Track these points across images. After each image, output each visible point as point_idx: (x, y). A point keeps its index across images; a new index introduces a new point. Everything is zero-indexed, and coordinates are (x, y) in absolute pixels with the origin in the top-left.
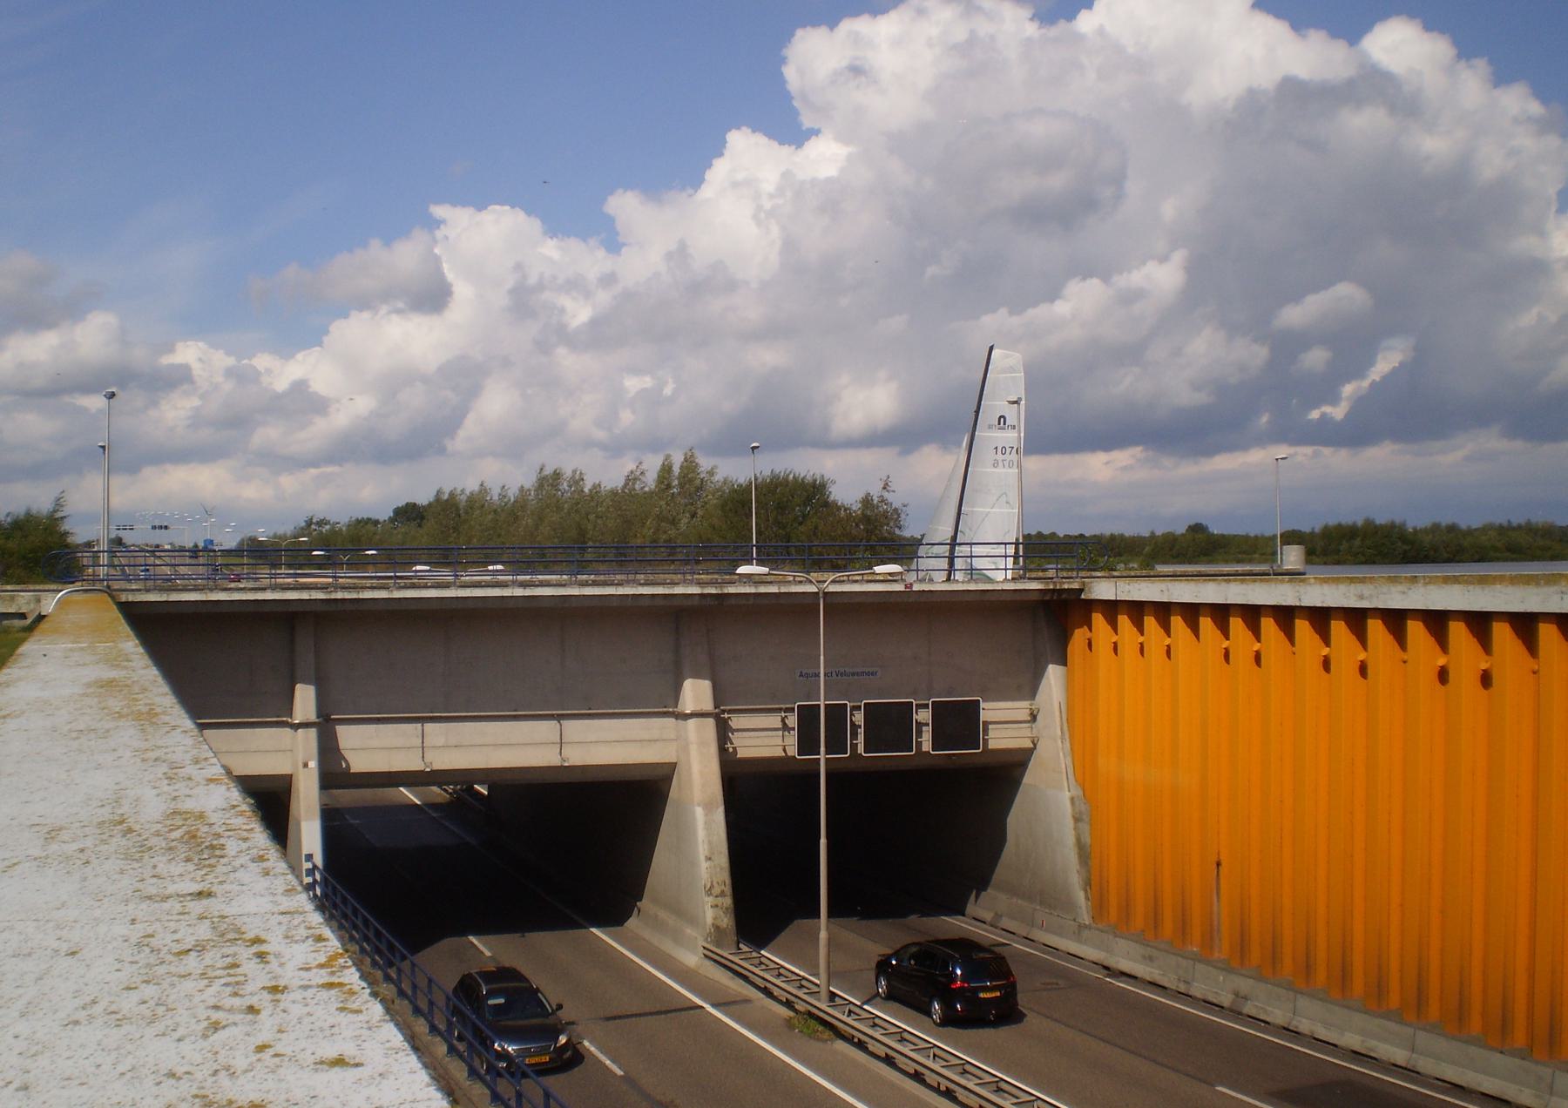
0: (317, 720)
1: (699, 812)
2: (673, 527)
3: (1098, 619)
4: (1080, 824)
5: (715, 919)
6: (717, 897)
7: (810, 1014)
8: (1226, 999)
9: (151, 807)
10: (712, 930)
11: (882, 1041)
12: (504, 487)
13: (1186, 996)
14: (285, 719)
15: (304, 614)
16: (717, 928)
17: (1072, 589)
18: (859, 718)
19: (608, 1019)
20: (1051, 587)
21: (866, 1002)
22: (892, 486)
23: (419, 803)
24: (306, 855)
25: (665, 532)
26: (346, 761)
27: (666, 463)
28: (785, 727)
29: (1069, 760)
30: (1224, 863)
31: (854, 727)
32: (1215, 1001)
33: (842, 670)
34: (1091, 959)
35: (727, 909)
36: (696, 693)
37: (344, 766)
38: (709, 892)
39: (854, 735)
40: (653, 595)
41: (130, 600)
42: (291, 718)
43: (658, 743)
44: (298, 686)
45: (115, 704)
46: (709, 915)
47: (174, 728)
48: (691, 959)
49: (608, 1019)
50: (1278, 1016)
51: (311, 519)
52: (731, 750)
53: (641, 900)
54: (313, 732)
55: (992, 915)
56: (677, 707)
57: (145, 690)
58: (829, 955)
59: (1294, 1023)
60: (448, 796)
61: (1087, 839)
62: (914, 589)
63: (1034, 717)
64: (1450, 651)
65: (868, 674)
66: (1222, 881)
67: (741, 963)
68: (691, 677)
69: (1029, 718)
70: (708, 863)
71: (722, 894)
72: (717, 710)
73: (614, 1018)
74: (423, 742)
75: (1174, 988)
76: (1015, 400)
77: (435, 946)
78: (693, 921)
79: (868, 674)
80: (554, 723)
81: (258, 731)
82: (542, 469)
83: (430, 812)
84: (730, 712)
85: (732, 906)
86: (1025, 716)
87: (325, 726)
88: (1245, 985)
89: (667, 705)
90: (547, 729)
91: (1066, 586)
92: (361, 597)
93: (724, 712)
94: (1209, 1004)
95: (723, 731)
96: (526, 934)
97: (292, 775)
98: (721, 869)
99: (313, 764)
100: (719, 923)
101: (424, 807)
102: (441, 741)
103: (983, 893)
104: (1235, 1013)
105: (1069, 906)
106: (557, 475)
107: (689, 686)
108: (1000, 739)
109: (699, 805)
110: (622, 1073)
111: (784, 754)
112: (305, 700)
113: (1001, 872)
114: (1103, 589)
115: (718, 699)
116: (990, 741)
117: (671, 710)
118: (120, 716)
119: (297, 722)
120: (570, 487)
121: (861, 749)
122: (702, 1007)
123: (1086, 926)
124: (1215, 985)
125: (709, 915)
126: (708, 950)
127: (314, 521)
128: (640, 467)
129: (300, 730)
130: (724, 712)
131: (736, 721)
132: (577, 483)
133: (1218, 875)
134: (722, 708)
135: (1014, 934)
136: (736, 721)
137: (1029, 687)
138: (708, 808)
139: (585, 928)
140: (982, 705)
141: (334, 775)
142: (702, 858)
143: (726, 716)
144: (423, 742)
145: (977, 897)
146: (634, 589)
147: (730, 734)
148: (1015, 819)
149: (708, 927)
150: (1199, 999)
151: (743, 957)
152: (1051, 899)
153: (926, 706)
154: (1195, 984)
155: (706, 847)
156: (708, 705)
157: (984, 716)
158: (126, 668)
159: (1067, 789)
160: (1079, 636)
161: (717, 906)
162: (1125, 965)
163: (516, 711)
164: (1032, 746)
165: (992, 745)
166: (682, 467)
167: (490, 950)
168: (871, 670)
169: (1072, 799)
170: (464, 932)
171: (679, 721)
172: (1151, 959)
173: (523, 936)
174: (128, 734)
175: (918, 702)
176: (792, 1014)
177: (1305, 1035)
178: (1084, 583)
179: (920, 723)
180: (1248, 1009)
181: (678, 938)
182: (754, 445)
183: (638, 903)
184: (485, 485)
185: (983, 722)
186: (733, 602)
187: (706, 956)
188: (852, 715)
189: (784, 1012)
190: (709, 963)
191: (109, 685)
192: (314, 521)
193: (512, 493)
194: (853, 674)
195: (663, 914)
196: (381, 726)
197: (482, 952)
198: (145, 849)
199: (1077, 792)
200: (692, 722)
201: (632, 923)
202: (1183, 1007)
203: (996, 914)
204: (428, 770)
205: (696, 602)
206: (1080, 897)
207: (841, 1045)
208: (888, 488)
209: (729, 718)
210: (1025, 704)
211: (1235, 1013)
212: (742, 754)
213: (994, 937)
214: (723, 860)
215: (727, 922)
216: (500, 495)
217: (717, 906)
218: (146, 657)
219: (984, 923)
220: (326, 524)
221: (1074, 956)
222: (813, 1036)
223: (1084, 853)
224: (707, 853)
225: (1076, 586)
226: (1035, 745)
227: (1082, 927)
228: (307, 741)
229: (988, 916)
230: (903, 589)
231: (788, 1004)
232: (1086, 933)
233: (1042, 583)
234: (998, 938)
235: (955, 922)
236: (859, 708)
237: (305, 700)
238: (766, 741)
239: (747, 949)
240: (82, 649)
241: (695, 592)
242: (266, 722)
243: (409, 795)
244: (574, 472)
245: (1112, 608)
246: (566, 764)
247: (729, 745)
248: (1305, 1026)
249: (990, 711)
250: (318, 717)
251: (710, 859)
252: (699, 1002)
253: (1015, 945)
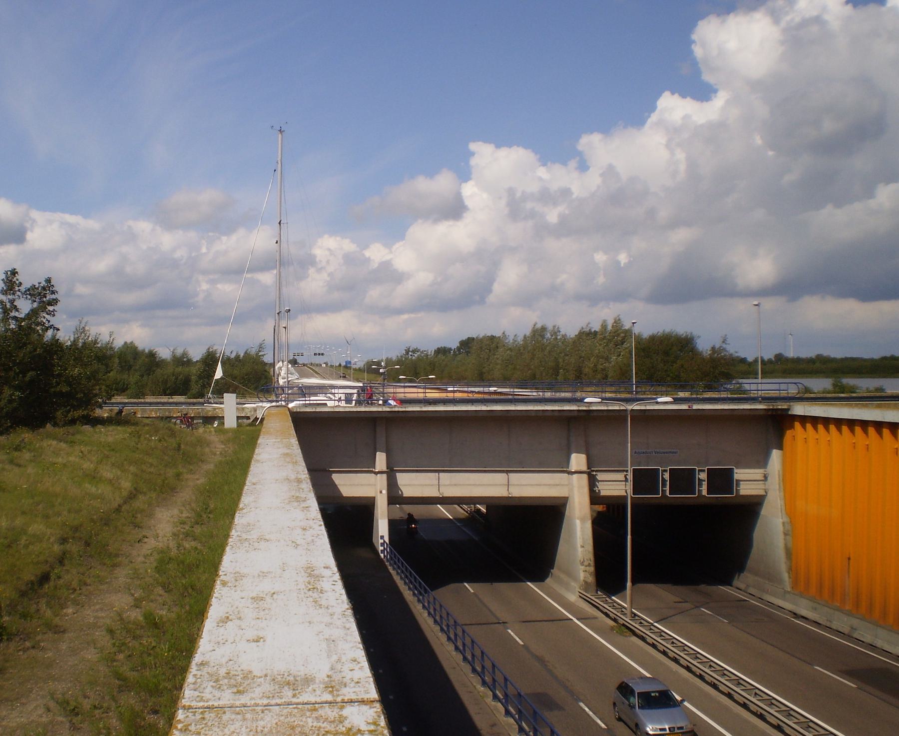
0: (387, 470)
1: (578, 522)
2: (606, 362)
3: (797, 425)
4: (788, 537)
5: (585, 577)
6: (586, 566)
7: (624, 625)
8: (846, 630)
9: (293, 477)
10: (583, 583)
11: (652, 637)
12: (516, 335)
13: (828, 629)
14: (371, 469)
15: (381, 418)
16: (586, 582)
17: (783, 409)
18: (667, 476)
19: (524, 622)
20: (771, 408)
21: (656, 622)
22: (728, 341)
23: (451, 518)
24: (381, 536)
25: (602, 364)
26: (401, 491)
27: (604, 324)
28: (626, 480)
29: (783, 503)
30: (852, 558)
31: (664, 480)
32: (842, 631)
33: (658, 450)
34: (789, 609)
35: (591, 573)
36: (578, 461)
37: (400, 493)
38: (582, 564)
39: (664, 485)
40: (553, 410)
41: (298, 411)
42: (375, 469)
43: (558, 486)
44: (378, 453)
45: (288, 460)
46: (582, 576)
47: (300, 465)
48: (573, 598)
49: (524, 622)
50: (868, 639)
51: (409, 349)
52: (597, 491)
53: (553, 569)
54: (385, 476)
55: (745, 585)
56: (568, 468)
57: (296, 456)
58: (632, 595)
59: (876, 642)
60: (467, 515)
61: (790, 545)
62: (694, 408)
63: (766, 478)
64: (784, 448)
65: (673, 453)
66: (851, 568)
67: (595, 600)
68: (574, 453)
69: (763, 479)
70: (582, 549)
71: (589, 565)
72: (588, 470)
73: (525, 622)
74: (439, 483)
75: (824, 624)
76: (757, 304)
77: (447, 586)
78: (575, 579)
79: (673, 453)
80: (504, 475)
81: (359, 475)
82: (535, 325)
83: (456, 522)
84: (597, 471)
85: (595, 572)
86: (760, 477)
87: (391, 474)
88: (855, 622)
89: (563, 467)
90: (500, 478)
91: (780, 407)
92: (407, 410)
93: (593, 471)
94: (839, 633)
95: (592, 482)
96: (493, 584)
97: (374, 497)
98: (589, 552)
99: (384, 492)
100: (587, 580)
101: (454, 520)
102: (448, 482)
103: (742, 574)
104: (849, 637)
105: (780, 581)
106: (544, 329)
107: (574, 456)
108: (746, 490)
109: (578, 519)
110: (522, 643)
111: (626, 494)
112: (381, 460)
113: (750, 563)
114: (799, 409)
115: (590, 464)
116: (741, 490)
117: (565, 469)
118: (289, 462)
119: (377, 471)
120: (552, 336)
121: (668, 493)
122: (572, 619)
123: (789, 592)
124: (842, 623)
125: (582, 576)
126: (581, 593)
127: (411, 350)
128: (589, 326)
129: (378, 475)
130: (593, 471)
131: (600, 476)
132: (555, 333)
133: (849, 564)
134: (592, 469)
135: (754, 596)
136: (600, 476)
137: (762, 461)
138: (583, 520)
139: (524, 582)
140: (736, 471)
141: (395, 498)
142: (579, 546)
143: (594, 473)
144: (439, 483)
145: (739, 575)
146: (543, 407)
147: (597, 483)
148: (757, 534)
149: (581, 581)
150: (834, 630)
151: (599, 598)
152: (772, 577)
153: (704, 471)
154: (834, 622)
155: (581, 540)
156: (584, 468)
157: (736, 477)
158: (291, 449)
159: (781, 517)
160: (789, 434)
161: (586, 571)
162: (804, 613)
163: (485, 468)
164: (765, 494)
165: (742, 492)
166: (613, 326)
167: (473, 590)
168: (675, 451)
169: (783, 523)
170: (462, 581)
171: (570, 475)
172: (815, 609)
173: (492, 584)
174: (290, 466)
175: (663, 469)
176: (615, 624)
177: (879, 648)
178: (790, 406)
179: (701, 480)
180: (855, 635)
181: (568, 588)
182: (633, 321)
183: (552, 570)
184: (505, 333)
185: (736, 480)
186: (595, 414)
187: (580, 597)
188: (662, 475)
189: (612, 623)
190: (580, 600)
191: (287, 454)
192: (411, 350)
193: (520, 339)
194: (664, 453)
195: (562, 576)
196: (418, 474)
197: (469, 591)
198: (291, 481)
199: (786, 519)
200: (575, 476)
201: (549, 580)
202: (824, 633)
203: (747, 585)
204: (441, 496)
205: (576, 414)
206: (786, 576)
207: (634, 639)
208: (726, 342)
209: (596, 474)
210: (762, 471)
211: (849, 637)
212: (603, 493)
213: (743, 597)
214: (590, 547)
215: (591, 579)
216: (513, 340)
217: (586, 571)
218: (298, 445)
219: (741, 590)
220: (418, 352)
221: (781, 608)
222: (622, 634)
223: (789, 553)
224: (581, 544)
225: (785, 407)
226: (766, 492)
227: (786, 592)
228: (381, 481)
229: (742, 586)
230: (687, 408)
231: (615, 620)
232: (788, 596)
233: (766, 405)
234: (743, 597)
235: (725, 589)
236: (666, 471)
237: (381, 460)
238: (617, 487)
239: (601, 594)
240: (278, 442)
241: (575, 409)
242: (362, 471)
243: (444, 511)
244: (554, 327)
245: (804, 420)
246: (510, 496)
247: (596, 489)
248: (879, 643)
249: (740, 474)
250: (387, 469)
251: (583, 547)
252: (571, 617)
253: (752, 601)
